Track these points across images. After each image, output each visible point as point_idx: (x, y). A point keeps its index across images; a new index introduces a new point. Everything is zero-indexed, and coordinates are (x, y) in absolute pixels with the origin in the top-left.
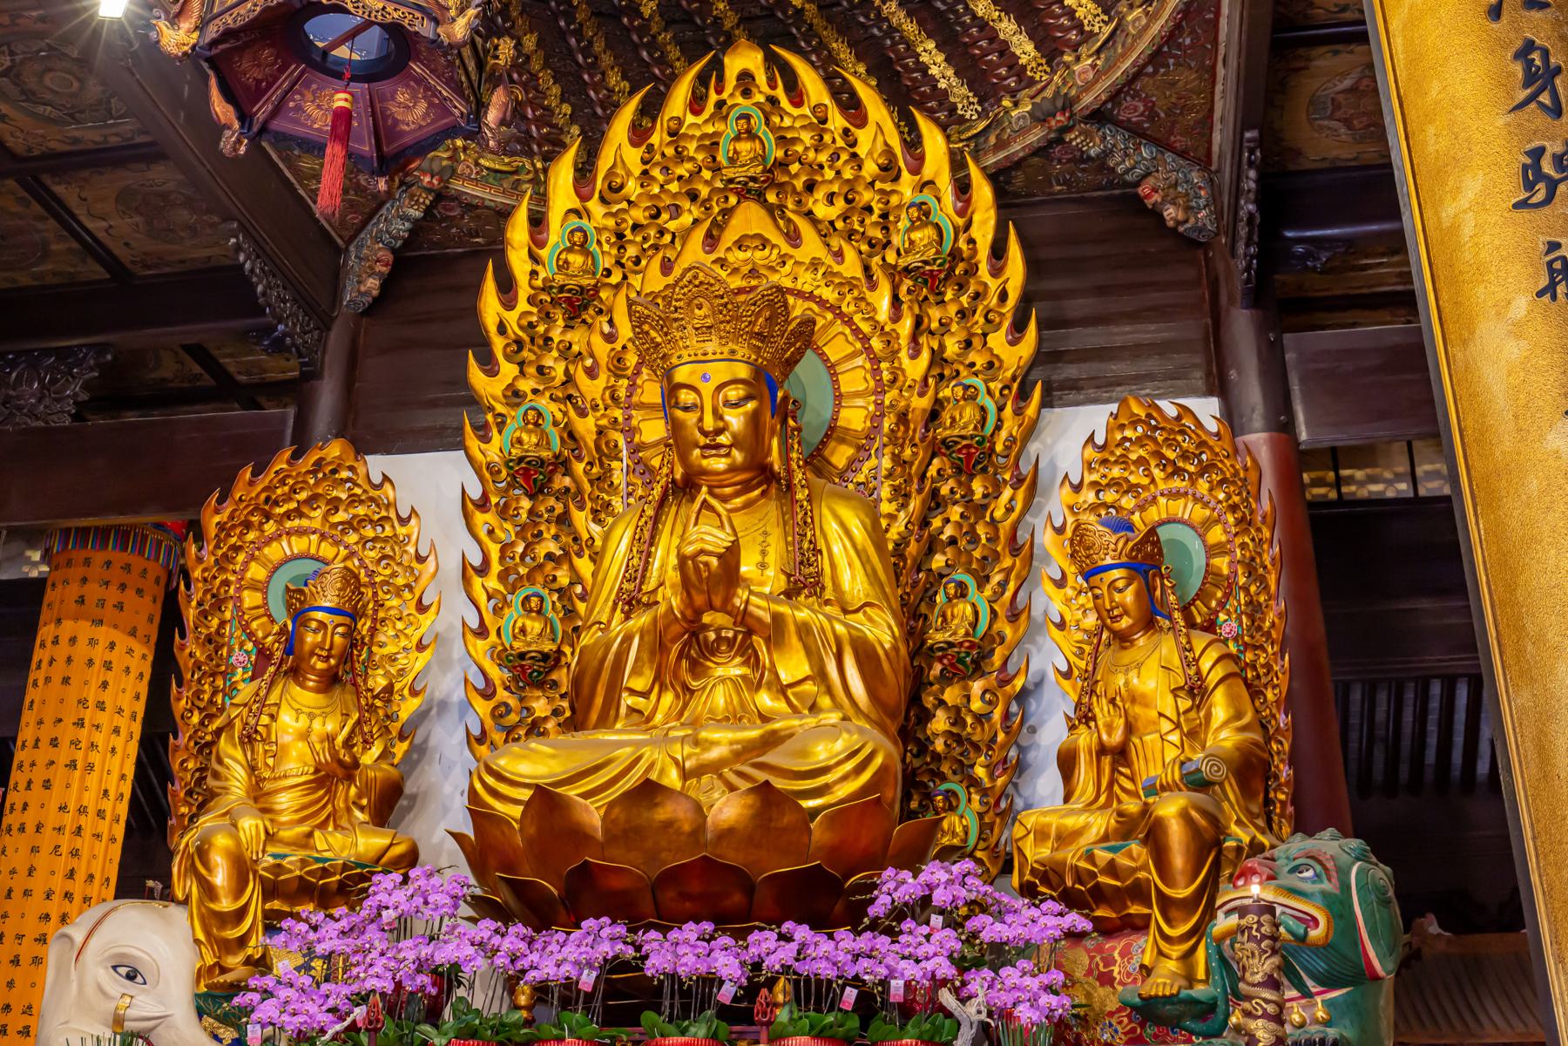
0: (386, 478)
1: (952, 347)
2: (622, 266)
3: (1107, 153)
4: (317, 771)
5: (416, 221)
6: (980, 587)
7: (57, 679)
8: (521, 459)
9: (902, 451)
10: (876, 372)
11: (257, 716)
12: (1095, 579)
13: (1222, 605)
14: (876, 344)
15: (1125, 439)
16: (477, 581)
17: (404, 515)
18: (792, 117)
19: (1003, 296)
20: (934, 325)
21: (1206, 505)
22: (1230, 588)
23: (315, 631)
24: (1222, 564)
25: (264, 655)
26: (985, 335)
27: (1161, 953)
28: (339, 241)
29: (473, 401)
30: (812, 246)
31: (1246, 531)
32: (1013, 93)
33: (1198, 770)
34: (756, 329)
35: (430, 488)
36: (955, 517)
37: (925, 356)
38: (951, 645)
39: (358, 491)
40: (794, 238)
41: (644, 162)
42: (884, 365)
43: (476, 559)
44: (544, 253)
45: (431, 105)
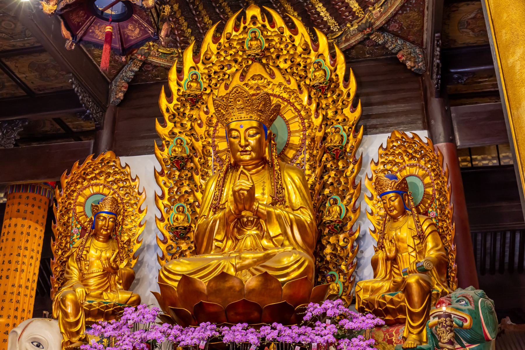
0: (127, 165)
1: (330, 114)
4: (104, 271)
5: (136, 72)
7: (10, 239)
8: (175, 157)
10: (303, 123)
14: (303, 113)
15: (394, 146)
16: (160, 201)
19: (349, 95)
20: (324, 106)
21: (423, 169)
23: (102, 220)
24: (430, 190)
25: (84, 229)
26: (342, 109)
27: (410, 332)
28: (109, 80)
29: (158, 137)
30: (279, 78)
31: (438, 179)
32: (351, 22)
33: (423, 266)
34: (260, 108)
37: (321, 117)
38: (332, 221)
39: (117, 170)
40: (272, 75)
41: (218, 49)
42: (306, 121)
44: (182, 83)
45: (140, 30)
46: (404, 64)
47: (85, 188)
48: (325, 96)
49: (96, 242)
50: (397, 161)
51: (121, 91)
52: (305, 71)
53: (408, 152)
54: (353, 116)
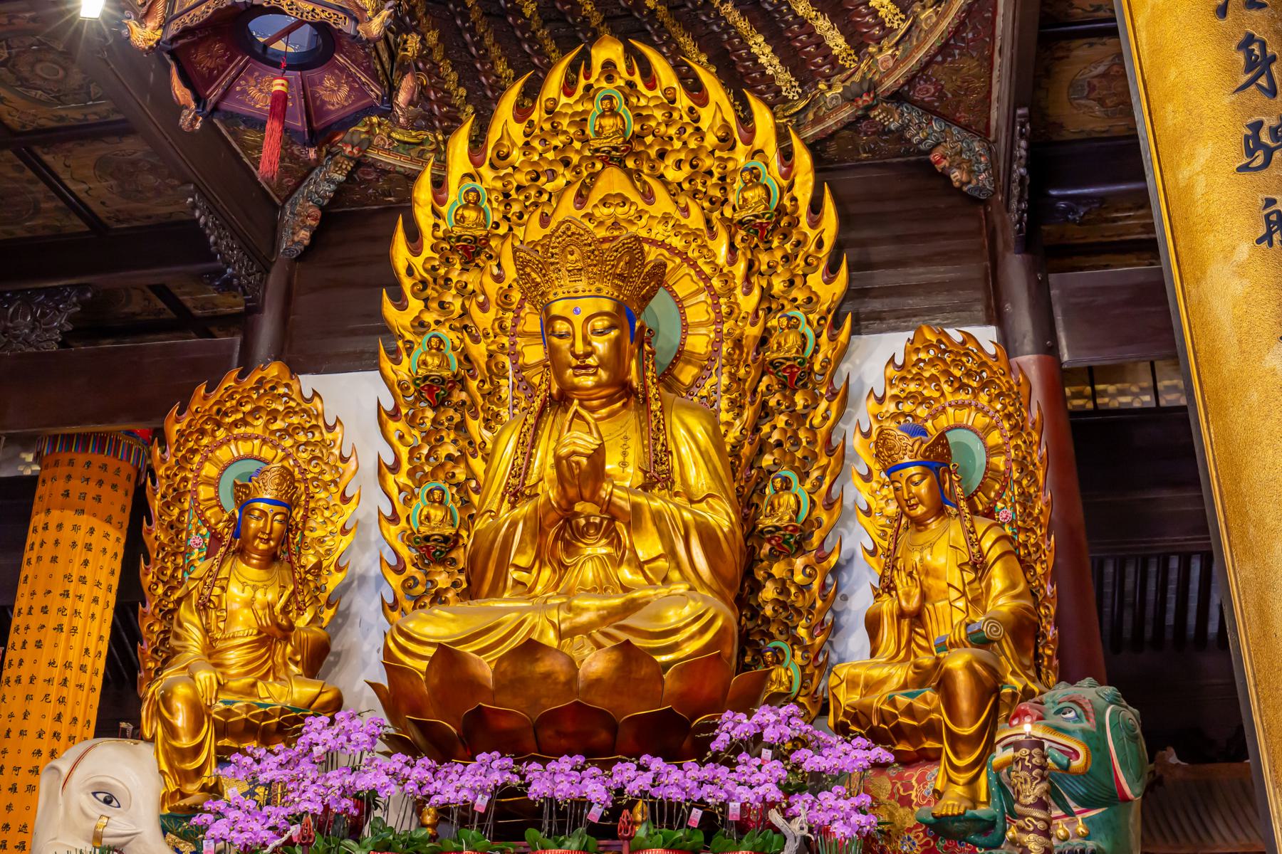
0: (315, 394)
1: (778, 285)
2: (509, 220)
3: (904, 127)
4: (259, 633)
5: (340, 184)
6: (802, 481)
8: (426, 378)
9: (737, 370)
10: (716, 306)
11: (211, 588)
12: (895, 475)
13: (999, 495)
14: (716, 283)
15: (920, 360)
16: (390, 478)
17: (331, 423)
18: (647, 98)
19: (820, 244)
20: (764, 268)
22: (1006, 481)
24: (999, 462)
25: (216, 538)
26: (805, 275)
27: (950, 780)
28: (277, 200)
29: (386, 331)
30: (663, 203)
31: (1019, 435)
32: (827, 78)
33: (981, 630)
35: (352, 401)
36: (781, 424)
37: (756, 292)
38: (778, 528)
39: (292, 404)
40: (649, 197)
41: (526, 135)
43: (389, 460)
44: (444, 210)
45: (352, 89)
46: (945, 176)
47: (220, 445)
48: (767, 246)
49: (242, 566)
52: (724, 189)
54: (830, 291)
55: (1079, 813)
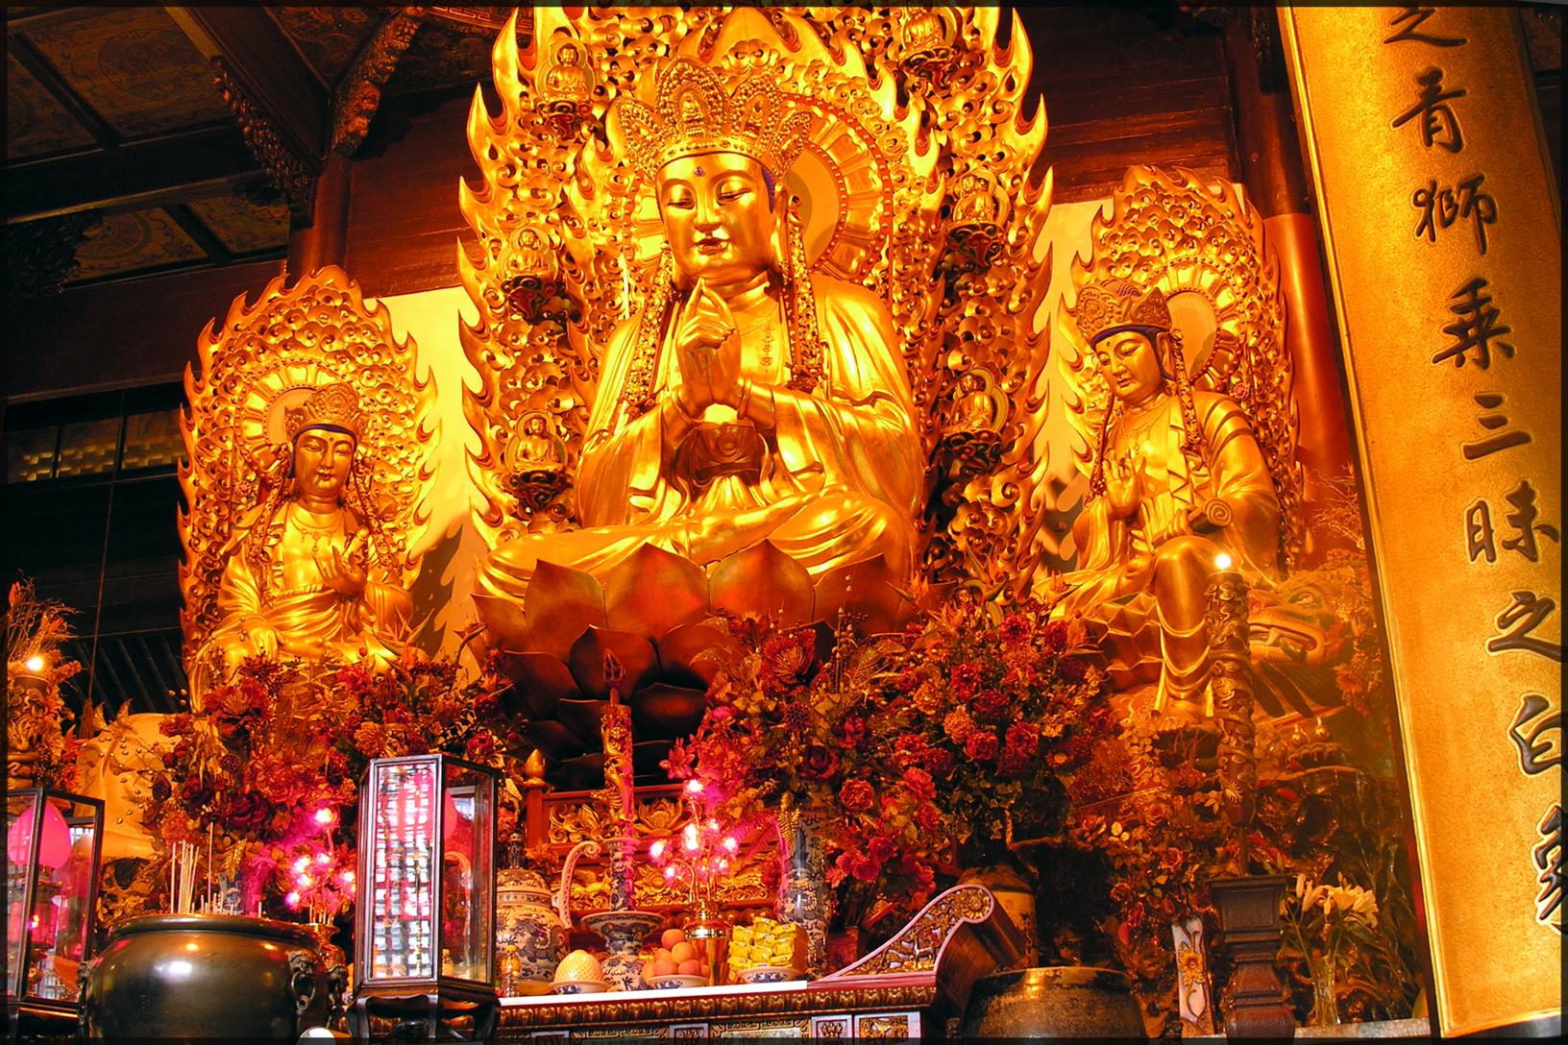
4: (324, 589)
5: (404, 52)
6: (998, 381)
8: (517, 280)
12: (1102, 345)
13: (1235, 367)
15: (1133, 211)
17: (400, 338)
21: (1214, 270)
22: (1242, 350)
24: (1230, 326)
25: (265, 485)
28: (326, 85)
30: (812, 45)
31: (1254, 291)
33: (1203, 515)
35: (431, 321)
36: (969, 312)
39: (354, 319)
44: (536, 73)
48: (945, 92)
50: (1146, 253)
51: (361, 114)
53: (1172, 226)
55: (1319, 712)
